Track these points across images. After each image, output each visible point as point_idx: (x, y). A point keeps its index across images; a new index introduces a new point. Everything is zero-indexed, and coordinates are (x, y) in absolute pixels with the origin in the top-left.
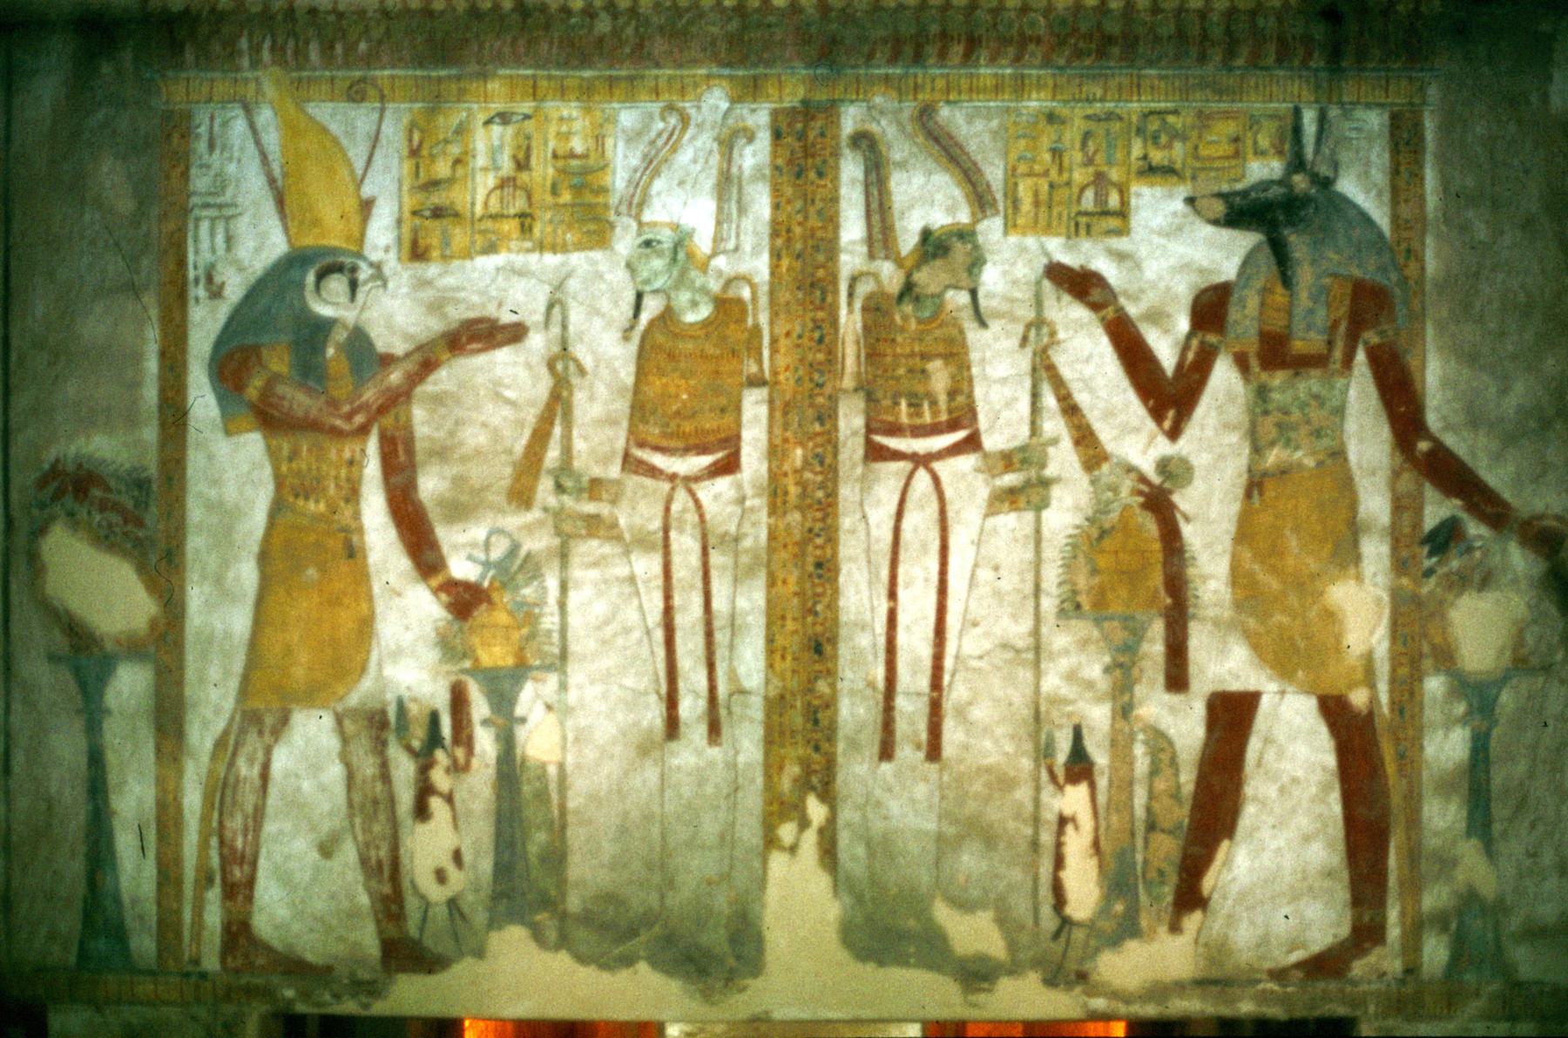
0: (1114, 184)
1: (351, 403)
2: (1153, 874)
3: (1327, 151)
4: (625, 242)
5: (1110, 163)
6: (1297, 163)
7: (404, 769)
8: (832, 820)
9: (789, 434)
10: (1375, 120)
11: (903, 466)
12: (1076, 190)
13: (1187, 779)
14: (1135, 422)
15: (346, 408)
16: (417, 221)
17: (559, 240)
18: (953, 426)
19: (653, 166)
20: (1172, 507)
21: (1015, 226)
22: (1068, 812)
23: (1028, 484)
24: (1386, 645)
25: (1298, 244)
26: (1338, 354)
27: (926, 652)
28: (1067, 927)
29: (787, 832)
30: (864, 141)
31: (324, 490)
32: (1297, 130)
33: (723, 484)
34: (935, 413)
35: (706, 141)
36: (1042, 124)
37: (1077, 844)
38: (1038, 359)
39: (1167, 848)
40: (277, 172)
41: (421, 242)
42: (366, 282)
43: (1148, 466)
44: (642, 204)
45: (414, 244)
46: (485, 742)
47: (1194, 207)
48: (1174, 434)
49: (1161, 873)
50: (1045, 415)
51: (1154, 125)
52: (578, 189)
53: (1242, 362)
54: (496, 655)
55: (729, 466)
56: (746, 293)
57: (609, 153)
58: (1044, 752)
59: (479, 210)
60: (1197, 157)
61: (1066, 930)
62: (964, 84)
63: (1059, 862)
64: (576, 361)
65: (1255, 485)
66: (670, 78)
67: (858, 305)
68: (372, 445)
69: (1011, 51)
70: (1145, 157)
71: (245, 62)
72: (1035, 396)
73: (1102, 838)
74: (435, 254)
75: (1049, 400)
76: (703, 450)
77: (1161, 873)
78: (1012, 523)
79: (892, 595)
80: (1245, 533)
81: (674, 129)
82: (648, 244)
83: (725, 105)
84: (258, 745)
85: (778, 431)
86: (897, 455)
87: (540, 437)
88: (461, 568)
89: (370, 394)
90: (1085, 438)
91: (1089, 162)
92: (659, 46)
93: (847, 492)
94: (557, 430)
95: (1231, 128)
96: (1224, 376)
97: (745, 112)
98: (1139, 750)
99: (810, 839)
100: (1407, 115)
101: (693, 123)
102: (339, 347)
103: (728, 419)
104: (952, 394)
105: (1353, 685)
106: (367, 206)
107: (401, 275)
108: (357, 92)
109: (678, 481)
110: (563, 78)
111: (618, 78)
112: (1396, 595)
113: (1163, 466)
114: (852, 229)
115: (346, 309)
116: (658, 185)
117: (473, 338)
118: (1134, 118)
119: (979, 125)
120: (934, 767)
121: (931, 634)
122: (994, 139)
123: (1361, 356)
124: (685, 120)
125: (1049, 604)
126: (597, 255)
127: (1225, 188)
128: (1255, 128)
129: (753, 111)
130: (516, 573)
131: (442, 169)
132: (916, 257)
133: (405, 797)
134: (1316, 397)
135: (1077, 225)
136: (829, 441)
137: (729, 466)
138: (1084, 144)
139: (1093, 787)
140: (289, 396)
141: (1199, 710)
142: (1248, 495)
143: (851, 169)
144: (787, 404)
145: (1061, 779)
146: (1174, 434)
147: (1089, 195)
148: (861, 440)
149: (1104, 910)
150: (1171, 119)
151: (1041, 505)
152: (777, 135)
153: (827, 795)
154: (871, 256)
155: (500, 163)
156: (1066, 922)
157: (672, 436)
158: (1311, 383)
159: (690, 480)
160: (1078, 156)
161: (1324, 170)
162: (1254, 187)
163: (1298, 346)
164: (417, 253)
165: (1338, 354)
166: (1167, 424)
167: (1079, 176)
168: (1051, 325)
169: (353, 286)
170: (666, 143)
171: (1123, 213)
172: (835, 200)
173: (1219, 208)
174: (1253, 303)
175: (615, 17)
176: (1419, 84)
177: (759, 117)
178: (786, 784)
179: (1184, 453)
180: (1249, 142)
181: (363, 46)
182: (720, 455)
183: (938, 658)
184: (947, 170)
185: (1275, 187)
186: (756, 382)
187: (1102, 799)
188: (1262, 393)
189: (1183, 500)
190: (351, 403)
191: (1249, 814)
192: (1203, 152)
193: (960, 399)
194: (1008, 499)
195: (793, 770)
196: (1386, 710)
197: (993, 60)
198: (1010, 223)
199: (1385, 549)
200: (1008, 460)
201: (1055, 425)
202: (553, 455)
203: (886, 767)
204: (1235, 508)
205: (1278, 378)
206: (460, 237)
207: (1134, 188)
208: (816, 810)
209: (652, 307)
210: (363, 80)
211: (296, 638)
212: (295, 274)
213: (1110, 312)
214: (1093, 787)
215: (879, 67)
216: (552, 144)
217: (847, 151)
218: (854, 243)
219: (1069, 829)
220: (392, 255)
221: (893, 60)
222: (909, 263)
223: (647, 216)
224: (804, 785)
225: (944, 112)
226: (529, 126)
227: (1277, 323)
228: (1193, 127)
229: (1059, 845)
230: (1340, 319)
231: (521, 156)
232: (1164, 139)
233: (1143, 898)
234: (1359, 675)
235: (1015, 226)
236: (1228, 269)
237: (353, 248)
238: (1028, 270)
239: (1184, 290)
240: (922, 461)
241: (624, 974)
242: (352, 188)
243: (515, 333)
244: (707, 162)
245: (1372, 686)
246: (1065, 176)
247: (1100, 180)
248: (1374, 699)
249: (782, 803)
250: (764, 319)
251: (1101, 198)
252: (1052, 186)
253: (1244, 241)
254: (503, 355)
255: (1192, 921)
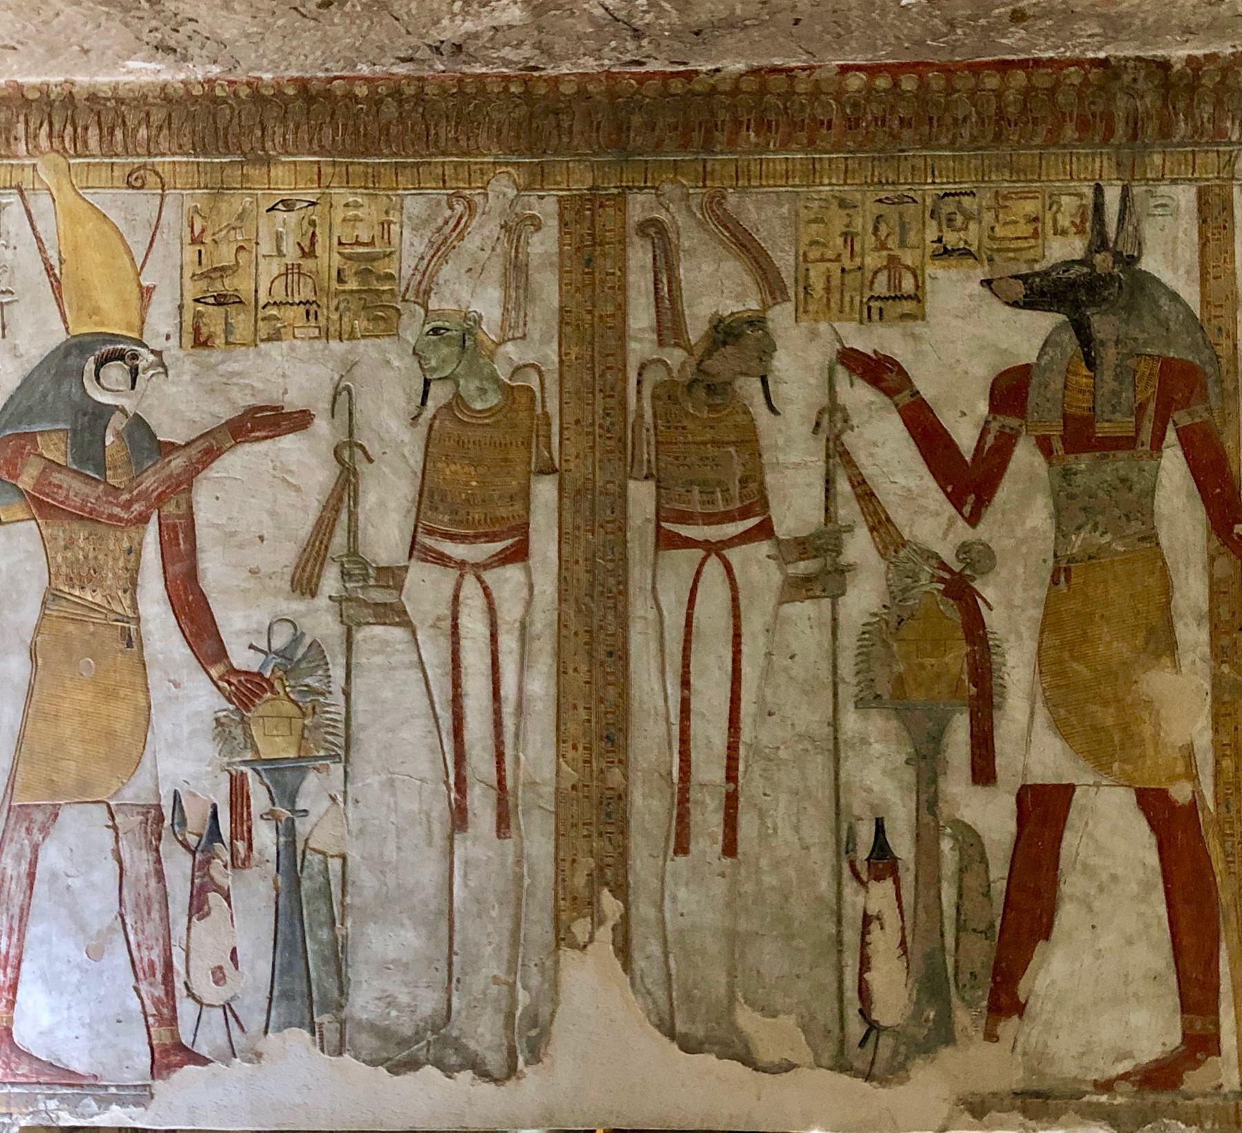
0: (908, 268)
1: (131, 492)
2: (965, 978)
3: (1130, 228)
4: (412, 329)
5: (902, 244)
6: (1100, 243)
7: (178, 867)
8: (625, 917)
9: (579, 521)
10: (1185, 196)
11: (699, 553)
12: (869, 275)
13: (999, 872)
14: (933, 507)
15: (126, 496)
16: (200, 308)
17: (346, 328)
18: (745, 514)
19: (441, 249)
20: (974, 593)
21: (806, 312)
22: (873, 910)
23: (824, 572)
24: (1208, 735)
25: (1102, 325)
26: (1146, 436)
27: (720, 740)
28: (874, 1032)
29: (581, 928)
30: (654, 230)
31: (103, 579)
32: (1099, 208)
33: (513, 572)
34: (727, 501)
35: (493, 228)
36: (834, 206)
37: (884, 942)
38: (831, 445)
39: (980, 952)
40: (54, 261)
41: (204, 330)
42: (145, 370)
43: (947, 553)
44: (427, 293)
45: (197, 331)
46: (265, 837)
47: (991, 289)
48: (973, 520)
49: (973, 975)
50: (840, 499)
51: (949, 206)
52: (364, 274)
53: (1045, 446)
54: (279, 746)
55: (519, 554)
56: (534, 383)
57: (395, 240)
58: (845, 846)
59: (263, 300)
60: (992, 238)
61: (872, 1037)
62: (754, 168)
63: (865, 964)
64: (362, 447)
65: (1061, 572)
66: (457, 165)
67: (647, 392)
68: (152, 529)
69: (803, 136)
70: (940, 240)
71: (22, 147)
72: (829, 482)
73: (909, 939)
74: (220, 341)
75: (843, 486)
76: (491, 537)
77: (973, 975)
78: (804, 611)
79: (685, 684)
80: (1050, 622)
81: (461, 218)
82: (435, 331)
83: (512, 193)
84: (26, 842)
85: (567, 516)
86: (689, 543)
87: (324, 528)
88: (242, 658)
89: (149, 482)
90: (880, 524)
91: (883, 246)
92: (446, 131)
93: (639, 575)
94: (344, 516)
95: (1030, 207)
96: (1025, 456)
97: (533, 200)
98: (946, 845)
99: (605, 934)
100: (1217, 190)
101: (480, 210)
102: (118, 434)
103: (518, 507)
104: (744, 481)
105: (1173, 778)
106: (146, 293)
107: (182, 360)
108: (136, 179)
109: (467, 568)
110: (347, 165)
111: (404, 166)
112: (1217, 683)
113: (964, 549)
114: (641, 317)
115: (128, 397)
116: (446, 271)
117: (259, 424)
118: (929, 201)
119: (769, 211)
120: (728, 861)
121: (725, 724)
122: (784, 227)
123: (1171, 436)
124: (471, 207)
125: (848, 692)
126: (385, 342)
127: (1024, 270)
128: (1055, 208)
129: (541, 198)
130: (299, 661)
131: (226, 256)
132: (705, 345)
133: (180, 892)
134: (1123, 480)
135: (869, 309)
136: (620, 529)
137: (519, 554)
138: (876, 229)
139: (897, 882)
140: (65, 485)
141: (1010, 802)
142: (1055, 581)
143: (640, 256)
144: (578, 492)
145: (864, 877)
146: (973, 520)
147: (882, 278)
148: (651, 527)
149: (917, 1015)
150: (966, 201)
151: (836, 596)
152: (563, 223)
153: (621, 890)
154: (661, 343)
155: (284, 250)
156: (873, 1027)
157: (460, 523)
158: (1120, 463)
159: (479, 568)
160: (871, 240)
161: (1128, 250)
162: (1054, 267)
163: (1103, 429)
164: (201, 342)
165: (1146, 436)
166: (967, 510)
167: (873, 260)
168: (844, 409)
169: (134, 372)
170: (454, 230)
171: (917, 298)
172: (623, 288)
173: (1019, 289)
174: (1057, 383)
175: (400, 103)
176: (1227, 157)
177: (546, 207)
178: (580, 880)
179: (984, 538)
180: (1049, 223)
181: (143, 132)
182: (510, 542)
183: (733, 748)
184: (737, 257)
185: (1077, 267)
186: (547, 469)
187: (908, 897)
188: (1067, 474)
189: (988, 590)
190: (131, 492)
191: (1067, 916)
192: (1000, 232)
193: (753, 486)
194: (800, 588)
195: (587, 863)
196: (1210, 804)
197: (784, 146)
198: (801, 309)
199: (1204, 636)
200: (803, 547)
201: (848, 510)
202: (340, 539)
203: (681, 859)
204: (1041, 593)
205: (1083, 462)
206: (242, 322)
207: (929, 270)
208: (610, 904)
209: (440, 394)
210: (143, 166)
211: (68, 732)
212: (72, 361)
213: (904, 398)
214: (897, 882)
215: (667, 153)
216: (337, 232)
217: (636, 239)
218: (642, 330)
219: (875, 927)
220: (174, 341)
221: (684, 146)
222: (698, 352)
223: (433, 304)
224: (597, 879)
225: (732, 199)
226: (316, 214)
227: (1081, 405)
228: (989, 209)
229: (864, 944)
230: (1148, 399)
231: (306, 244)
232: (959, 219)
233: (955, 1001)
234: (1180, 768)
235: (806, 312)
236: (1027, 353)
237: (135, 335)
238: (820, 354)
239: (981, 372)
240: (714, 548)
241: (408, 1080)
242: (132, 276)
243: (300, 421)
244: (493, 249)
245: (1193, 777)
246: (858, 260)
247: (893, 262)
248: (1197, 793)
249: (575, 899)
250: (553, 406)
251: (894, 282)
252: (843, 270)
253: (1044, 322)
254: (288, 442)
255: (1007, 1028)
